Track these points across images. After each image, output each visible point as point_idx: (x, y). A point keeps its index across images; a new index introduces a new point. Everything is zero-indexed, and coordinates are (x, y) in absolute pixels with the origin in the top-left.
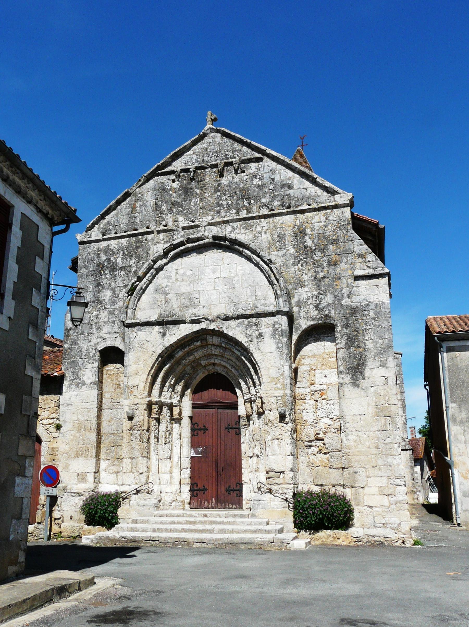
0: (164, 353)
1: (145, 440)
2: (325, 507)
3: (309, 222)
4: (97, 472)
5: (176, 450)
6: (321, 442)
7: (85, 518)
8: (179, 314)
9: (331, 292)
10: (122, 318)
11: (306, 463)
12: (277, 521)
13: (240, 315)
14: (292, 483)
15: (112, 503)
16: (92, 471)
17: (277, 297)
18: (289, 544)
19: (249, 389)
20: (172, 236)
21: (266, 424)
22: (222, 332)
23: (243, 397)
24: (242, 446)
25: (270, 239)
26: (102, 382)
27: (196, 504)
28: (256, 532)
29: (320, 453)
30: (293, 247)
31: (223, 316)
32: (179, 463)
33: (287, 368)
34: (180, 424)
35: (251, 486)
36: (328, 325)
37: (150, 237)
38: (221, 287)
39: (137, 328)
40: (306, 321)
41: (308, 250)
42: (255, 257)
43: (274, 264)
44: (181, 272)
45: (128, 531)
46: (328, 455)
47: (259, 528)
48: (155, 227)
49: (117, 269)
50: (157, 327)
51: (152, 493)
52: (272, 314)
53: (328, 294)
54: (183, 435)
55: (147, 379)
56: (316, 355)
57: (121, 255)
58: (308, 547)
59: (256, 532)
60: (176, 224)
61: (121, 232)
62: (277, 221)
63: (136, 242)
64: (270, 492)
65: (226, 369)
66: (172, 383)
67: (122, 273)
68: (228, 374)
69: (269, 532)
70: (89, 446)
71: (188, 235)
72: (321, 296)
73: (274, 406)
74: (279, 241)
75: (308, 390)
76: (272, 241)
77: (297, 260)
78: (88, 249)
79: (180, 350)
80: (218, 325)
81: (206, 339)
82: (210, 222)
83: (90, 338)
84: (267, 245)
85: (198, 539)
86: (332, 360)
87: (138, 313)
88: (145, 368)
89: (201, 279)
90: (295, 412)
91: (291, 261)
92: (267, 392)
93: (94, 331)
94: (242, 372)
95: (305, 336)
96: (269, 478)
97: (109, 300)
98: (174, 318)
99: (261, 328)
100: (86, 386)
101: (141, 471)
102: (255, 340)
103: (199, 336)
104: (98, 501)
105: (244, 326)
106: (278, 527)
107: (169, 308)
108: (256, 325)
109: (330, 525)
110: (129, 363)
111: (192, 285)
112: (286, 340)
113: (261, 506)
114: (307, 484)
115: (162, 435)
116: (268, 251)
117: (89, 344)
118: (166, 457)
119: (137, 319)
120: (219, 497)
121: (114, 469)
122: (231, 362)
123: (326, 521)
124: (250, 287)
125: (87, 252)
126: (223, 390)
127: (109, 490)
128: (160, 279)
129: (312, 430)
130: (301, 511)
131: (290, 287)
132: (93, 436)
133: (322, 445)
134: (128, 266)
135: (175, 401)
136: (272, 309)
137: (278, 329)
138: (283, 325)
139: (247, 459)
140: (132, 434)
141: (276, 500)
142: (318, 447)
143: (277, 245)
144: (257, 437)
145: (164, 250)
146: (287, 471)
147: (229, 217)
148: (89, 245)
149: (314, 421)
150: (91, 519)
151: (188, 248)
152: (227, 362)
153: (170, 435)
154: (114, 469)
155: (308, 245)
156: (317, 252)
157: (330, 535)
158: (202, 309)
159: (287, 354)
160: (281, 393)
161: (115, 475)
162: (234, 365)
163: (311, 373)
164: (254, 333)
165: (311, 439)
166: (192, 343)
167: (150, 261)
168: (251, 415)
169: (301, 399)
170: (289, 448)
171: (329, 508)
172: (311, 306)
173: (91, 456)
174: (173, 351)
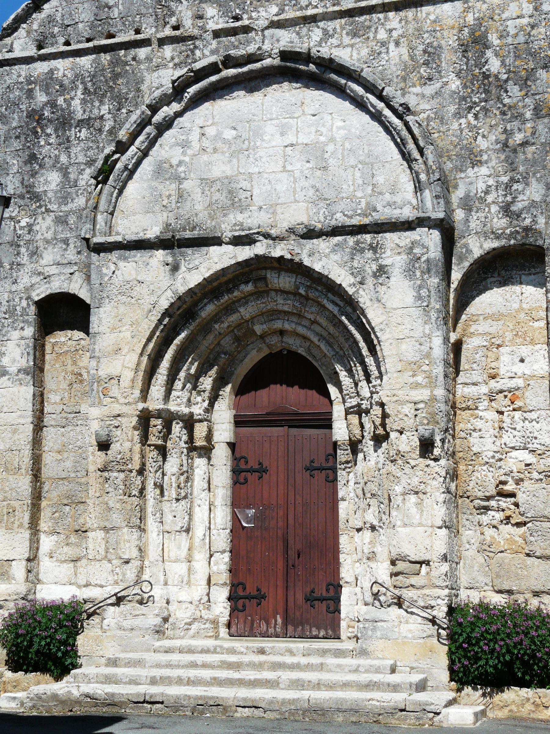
0: (176, 307)
1: (134, 493)
2: (517, 639)
3: (496, 17)
4: (33, 559)
5: (201, 514)
6: (508, 499)
7: (8, 654)
8: (206, 224)
9: (538, 175)
10: (85, 231)
11: (477, 544)
12: (414, 665)
13: (337, 227)
14: (447, 587)
15: (65, 623)
16: (21, 557)
17: (419, 188)
18: (438, 714)
19: (356, 385)
20: (192, 51)
21: (392, 461)
22: (300, 264)
23: (344, 402)
24: (340, 506)
25: (406, 57)
26: (42, 370)
27: (241, 626)
28: (369, 686)
29: (507, 524)
30: (458, 75)
31: (301, 230)
32: (207, 541)
33: (437, 342)
34: (209, 459)
35: (358, 590)
36: (528, 249)
37: (142, 52)
38: (298, 165)
39: (116, 254)
40: (482, 239)
41: (490, 83)
42: (372, 99)
43: (414, 114)
44: (211, 131)
45: (97, 682)
46: (523, 529)
47: (375, 680)
48: (154, 29)
49: (71, 126)
50: (161, 252)
51: (150, 604)
52: (408, 226)
53: (533, 181)
54: (214, 483)
55: (138, 364)
56: (502, 315)
57: (79, 92)
58: (479, 722)
59: (369, 686)
60: (200, 23)
61: (79, 42)
62: (424, 15)
63: (114, 63)
64: (399, 603)
65: (308, 344)
66: (193, 371)
67: (84, 133)
68: (311, 354)
69: (395, 688)
70: (16, 504)
71: (227, 48)
72: (515, 186)
73: (410, 423)
74: (426, 63)
75: (484, 389)
76: (411, 62)
77: (465, 106)
78: (7, 78)
79: (209, 302)
80: (291, 247)
81: (265, 279)
82: (276, 18)
83: (15, 274)
84: (399, 72)
85: (245, 699)
86: (537, 324)
87: (120, 222)
88: (135, 340)
89: (255, 148)
90: (453, 436)
91: (452, 109)
92: (395, 392)
93: (25, 259)
94: (341, 349)
95: (479, 274)
96: (397, 574)
97: (56, 192)
98: (196, 232)
99: (383, 256)
100: (7, 377)
101: (126, 557)
102: (370, 281)
103: (251, 271)
104: (35, 619)
105: (348, 250)
106: (416, 678)
107: (185, 210)
108: (374, 248)
109: (527, 678)
110: (101, 329)
111: (235, 161)
112: (437, 280)
113: (378, 634)
114: (477, 588)
115: (170, 481)
116: (402, 85)
117: (14, 288)
118: (178, 528)
119: (118, 234)
120: (291, 612)
121: (69, 552)
122: (318, 329)
123: (519, 669)
124: (360, 166)
125: (5, 86)
126: (300, 388)
127: (58, 597)
128: (167, 148)
129: (490, 475)
130: (466, 646)
131: (449, 165)
132: (24, 483)
133: (512, 507)
134: (95, 119)
135: (198, 410)
136: (407, 213)
137: (419, 258)
138: (432, 248)
139: (351, 534)
140: (107, 479)
141: (411, 621)
142: (503, 510)
143: (422, 71)
144: (372, 487)
145: (173, 82)
146: (435, 559)
147: (316, 7)
148: (7, 68)
149: (496, 455)
150: (20, 657)
151: (226, 78)
152: (309, 329)
153: (187, 481)
154: (69, 552)
155: (492, 69)
156: (510, 86)
157: (528, 699)
158: (256, 214)
159: (439, 311)
160: (423, 394)
161: (72, 565)
162: (325, 334)
163: (490, 354)
164: (368, 265)
165: (488, 494)
166: (236, 286)
167: (144, 107)
168: (360, 441)
169: (468, 408)
170: (440, 513)
171: (527, 642)
172: (494, 209)
173: (21, 526)
174: (195, 304)
